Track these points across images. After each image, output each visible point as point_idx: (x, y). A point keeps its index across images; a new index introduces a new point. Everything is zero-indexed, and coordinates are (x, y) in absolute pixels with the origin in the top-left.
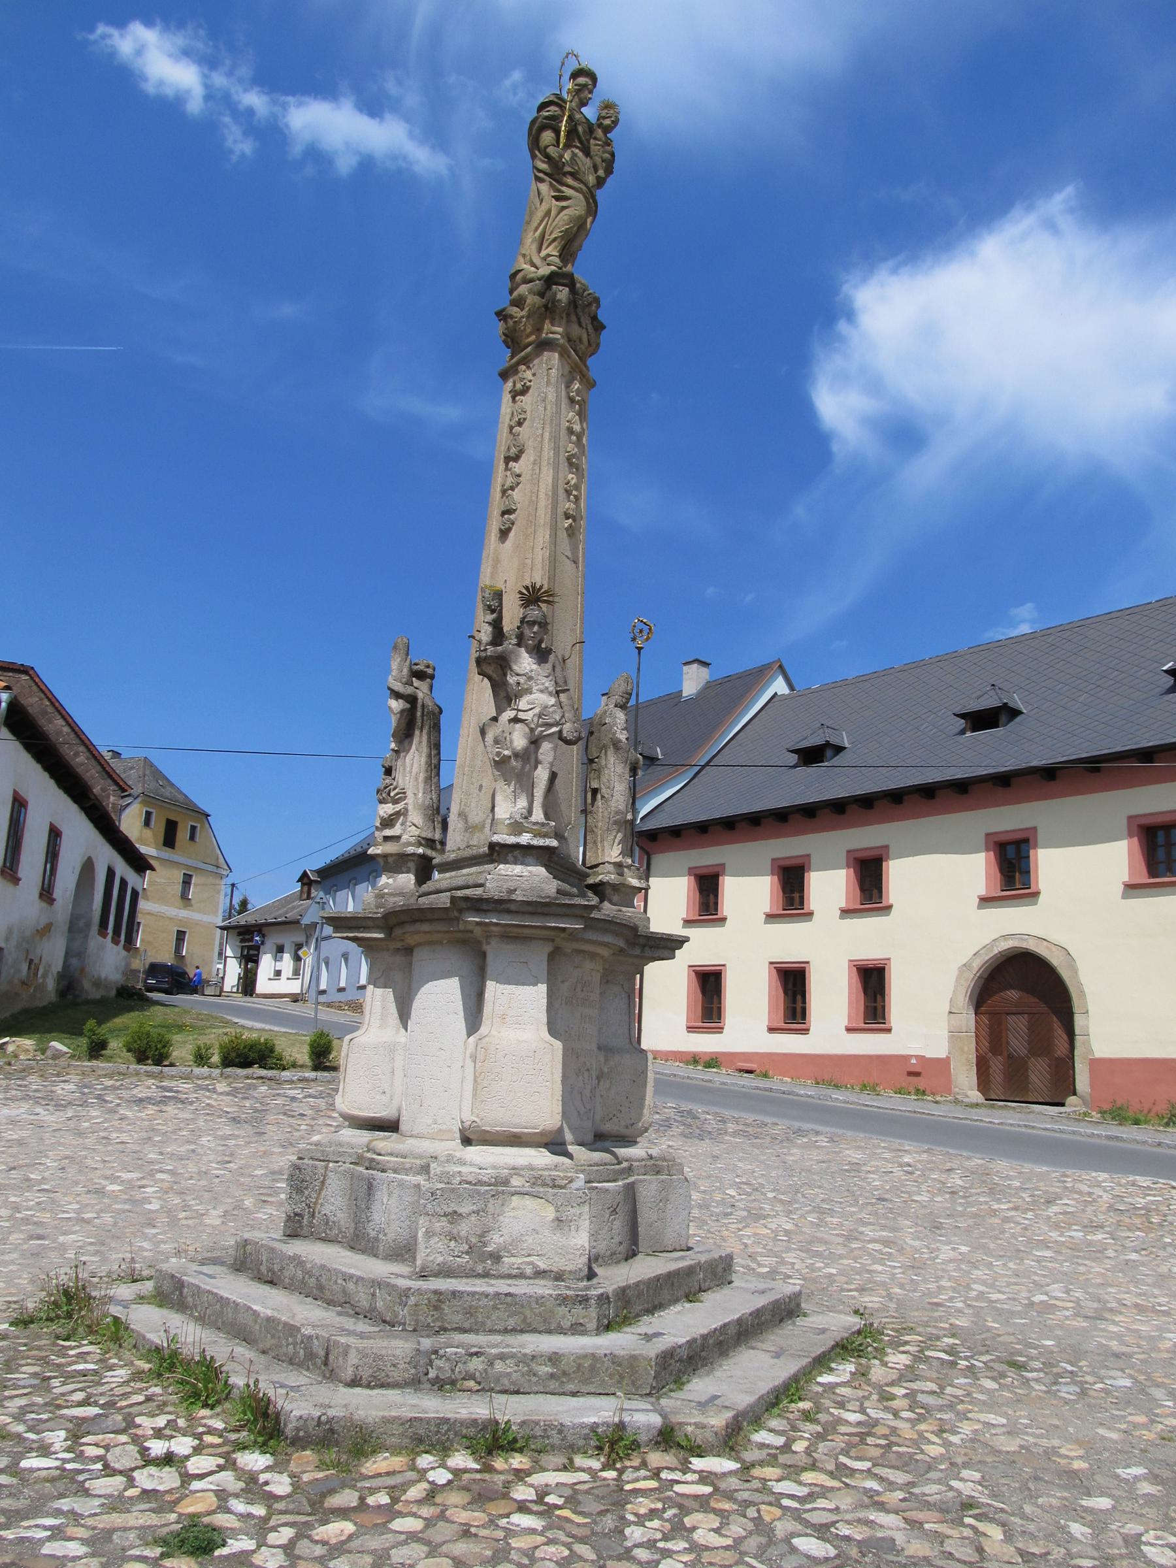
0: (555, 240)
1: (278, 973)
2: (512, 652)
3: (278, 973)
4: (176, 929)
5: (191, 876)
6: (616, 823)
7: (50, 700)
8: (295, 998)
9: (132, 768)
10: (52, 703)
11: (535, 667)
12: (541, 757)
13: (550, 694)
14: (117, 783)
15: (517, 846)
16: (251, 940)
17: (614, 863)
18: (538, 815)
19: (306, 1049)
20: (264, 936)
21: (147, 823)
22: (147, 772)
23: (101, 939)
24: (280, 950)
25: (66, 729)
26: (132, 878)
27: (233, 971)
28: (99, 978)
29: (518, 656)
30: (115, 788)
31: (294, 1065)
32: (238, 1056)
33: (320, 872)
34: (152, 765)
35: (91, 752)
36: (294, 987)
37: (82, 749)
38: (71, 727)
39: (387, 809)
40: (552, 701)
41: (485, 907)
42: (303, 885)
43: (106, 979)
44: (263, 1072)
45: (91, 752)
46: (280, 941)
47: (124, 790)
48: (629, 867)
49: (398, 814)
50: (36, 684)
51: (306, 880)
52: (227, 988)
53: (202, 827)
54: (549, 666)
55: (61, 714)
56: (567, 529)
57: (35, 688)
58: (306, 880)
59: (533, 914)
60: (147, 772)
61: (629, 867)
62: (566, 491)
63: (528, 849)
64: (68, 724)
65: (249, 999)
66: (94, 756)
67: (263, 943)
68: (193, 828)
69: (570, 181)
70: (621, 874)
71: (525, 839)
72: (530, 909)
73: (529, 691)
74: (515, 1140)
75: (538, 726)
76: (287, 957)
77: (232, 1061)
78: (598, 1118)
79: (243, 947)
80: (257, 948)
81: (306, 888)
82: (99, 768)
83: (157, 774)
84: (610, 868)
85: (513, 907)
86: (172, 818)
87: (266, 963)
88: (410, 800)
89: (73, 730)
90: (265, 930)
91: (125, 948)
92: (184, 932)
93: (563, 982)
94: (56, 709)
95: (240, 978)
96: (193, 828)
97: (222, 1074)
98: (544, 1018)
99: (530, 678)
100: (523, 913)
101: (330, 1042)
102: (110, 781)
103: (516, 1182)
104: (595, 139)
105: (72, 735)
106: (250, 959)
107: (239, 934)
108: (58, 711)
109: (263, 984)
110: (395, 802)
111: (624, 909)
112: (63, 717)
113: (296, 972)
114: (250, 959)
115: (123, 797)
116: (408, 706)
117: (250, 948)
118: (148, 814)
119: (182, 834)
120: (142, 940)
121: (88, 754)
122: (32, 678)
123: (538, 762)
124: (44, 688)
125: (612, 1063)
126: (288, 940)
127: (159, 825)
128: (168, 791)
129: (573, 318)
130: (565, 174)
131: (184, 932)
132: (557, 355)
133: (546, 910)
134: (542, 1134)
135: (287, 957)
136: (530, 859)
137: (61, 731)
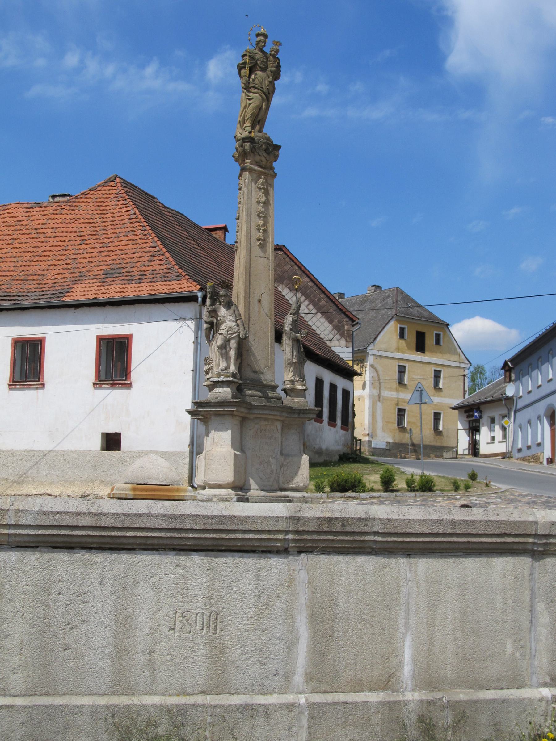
0: (248, 119)
1: (493, 438)
2: (218, 308)
3: (493, 438)
4: (433, 411)
5: (440, 372)
6: (289, 364)
7: (298, 266)
8: (504, 456)
9: (389, 297)
10: (299, 267)
11: (226, 312)
12: (231, 346)
13: (233, 321)
14: (347, 316)
15: (218, 382)
16: (472, 416)
17: (289, 381)
18: (233, 369)
19: (405, 483)
20: (481, 412)
21: (402, 336)
22: (399, 298)
23: (318, 424)
24: (493, 421)
25: (311, 284)
26: (341, 383)
27: (463, 441)
28: (320, 449)
29: (220, 308)
30: (347, 319)
31: (372, 490)
32: (339, 485)
33: (512, 360)
34: (402, 292)
35: (328, 297)
36: (501, 448)
37: (322, 296)
38: (314, 282)
39: (207, 367)
40: (234, 324)
41: (203, 405)
42: (506, 371)
43: (327, 449)
44: (354, 494)
45: (328, 297)
46: (492, 414)
47: (353, 321)
48: (297, 381)
49: (209, 369)
50: (288, 256)
51: (507, 368)
52: (460, 452)
53: (444, 335)
54: (232, 310)
55: (306, 274)
56: (259, 246)
57: (287, 259)
58: (507, 368)
59: (220, 406)
60: (399, 298)
61: (297, 381)
62: (258, 229)
63: (223, 382)
64: (312, 280)
65: (475, 459)
66: (330, 299)
67: (481, 417)
68: (438, 336)
69: (252, 90)
70: (294, 385)
71: (222, 378)
72: (218, 404)
73: (225, 322)
74: (220, 486)
75: (228, 335)
76: (497, 428)
77: (335, 489)
78: (281, 482)
79: (469, 421)
80: (478, 421)
81: (508, 373)
82: (335, 307)
83: (407, 298)
84: (288, 382)
85: (212, 404)
86: (421, 329)
87: (484, 435)
88: (214, 363)
89: (315, 284)
90: (482, 407)
91: (342, 428)
92: (440, 414)
93: (250, 430)
94: (303, 271)
95: (469, 444)
96: (438, 336)
97: (328, 496)
98: (230, 443)
99: (224, 317)
100: (217, 406)
101: (392, 475)
102: (343, 315)
103: (214, 499)
104: (269, 61)
105: (315, 287)
106: (474, 429)
107: (466, 412)
108: (304, 272)
109: (484, 449)
110: (209, 364)
111: (295, 398)
112: (307, 276)
113: (504, 437)
114: (474, 429)
115: (353, 326)
116: (209, 326)
117: (473, 421)
118: (402, 330)
119: (430, 341)
120: (408, 422)
121: (326, 299)
122: (285, 253)
123: (230, 348)
124: (293, 258)
125: (288, 461)
126: (496, 413)
127: (410, 336)
128: (415, 311)
129: (256, 153)
130: (250, 88)
131: (440, 414)
132: (247, 173)
133: (223, 404)
134: (228, 484)
135: (497, 428)
136: (225, 386)
137: (308, 285)
